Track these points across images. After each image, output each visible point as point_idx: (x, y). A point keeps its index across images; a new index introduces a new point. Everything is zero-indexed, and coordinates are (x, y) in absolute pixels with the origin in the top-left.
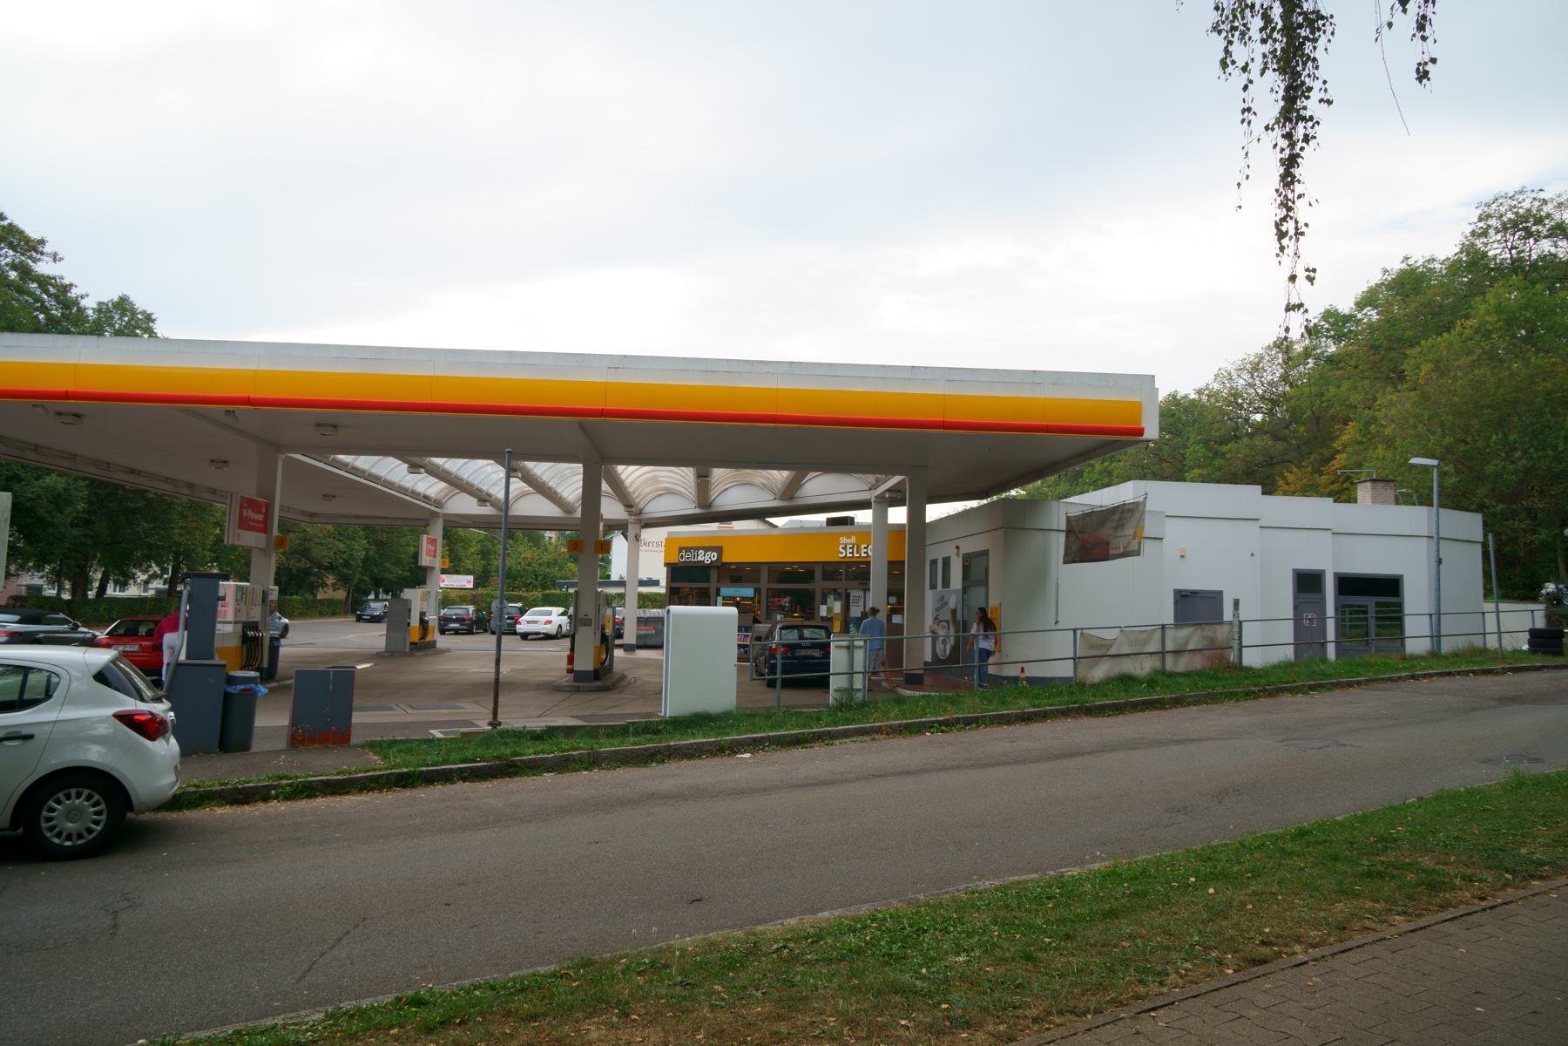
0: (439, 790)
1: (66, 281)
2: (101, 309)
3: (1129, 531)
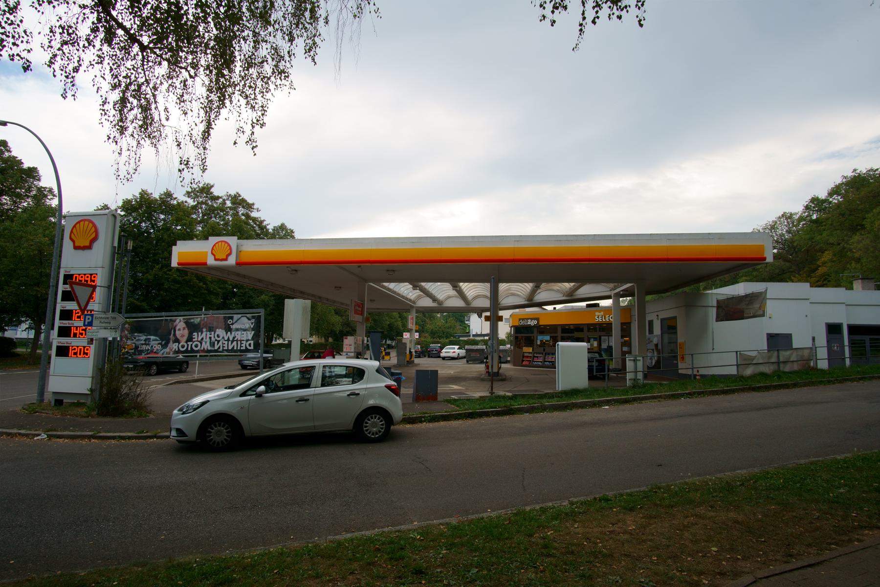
0: (484, 420)
1: (262, 219)
2: (276, 229)
3: (757, 306)
